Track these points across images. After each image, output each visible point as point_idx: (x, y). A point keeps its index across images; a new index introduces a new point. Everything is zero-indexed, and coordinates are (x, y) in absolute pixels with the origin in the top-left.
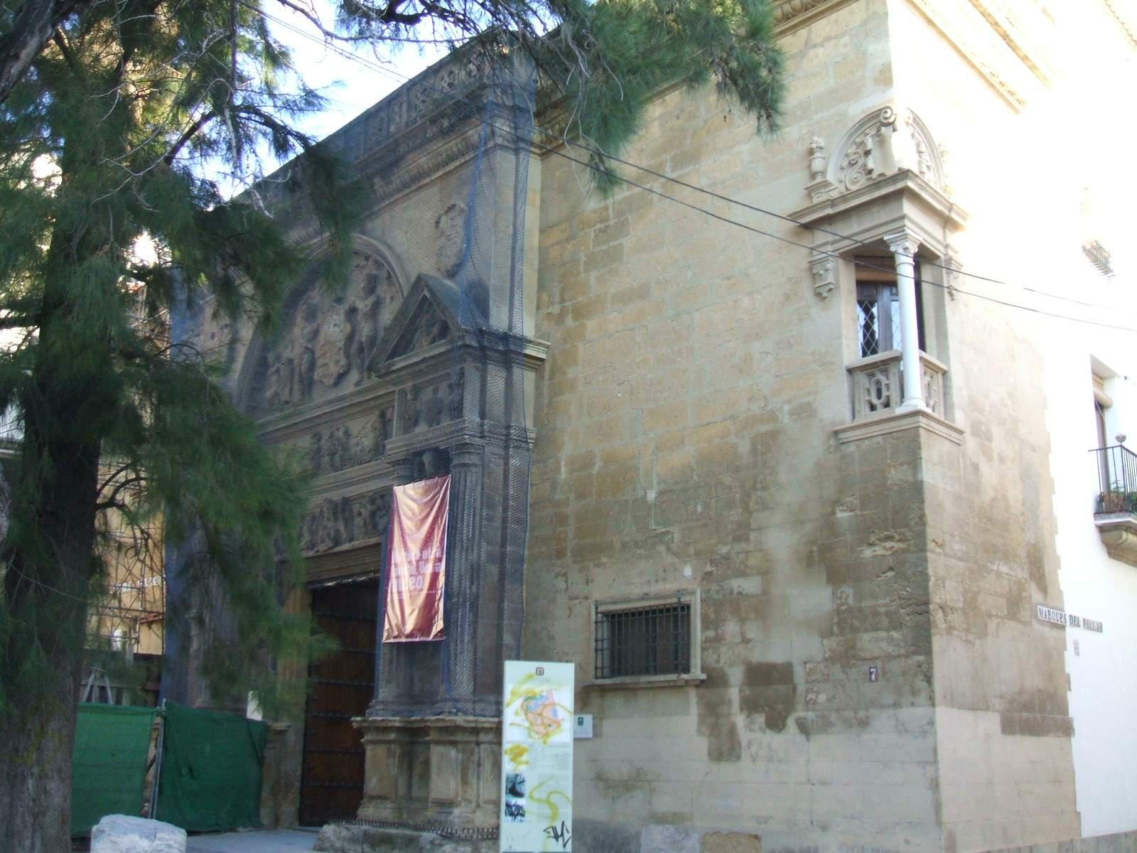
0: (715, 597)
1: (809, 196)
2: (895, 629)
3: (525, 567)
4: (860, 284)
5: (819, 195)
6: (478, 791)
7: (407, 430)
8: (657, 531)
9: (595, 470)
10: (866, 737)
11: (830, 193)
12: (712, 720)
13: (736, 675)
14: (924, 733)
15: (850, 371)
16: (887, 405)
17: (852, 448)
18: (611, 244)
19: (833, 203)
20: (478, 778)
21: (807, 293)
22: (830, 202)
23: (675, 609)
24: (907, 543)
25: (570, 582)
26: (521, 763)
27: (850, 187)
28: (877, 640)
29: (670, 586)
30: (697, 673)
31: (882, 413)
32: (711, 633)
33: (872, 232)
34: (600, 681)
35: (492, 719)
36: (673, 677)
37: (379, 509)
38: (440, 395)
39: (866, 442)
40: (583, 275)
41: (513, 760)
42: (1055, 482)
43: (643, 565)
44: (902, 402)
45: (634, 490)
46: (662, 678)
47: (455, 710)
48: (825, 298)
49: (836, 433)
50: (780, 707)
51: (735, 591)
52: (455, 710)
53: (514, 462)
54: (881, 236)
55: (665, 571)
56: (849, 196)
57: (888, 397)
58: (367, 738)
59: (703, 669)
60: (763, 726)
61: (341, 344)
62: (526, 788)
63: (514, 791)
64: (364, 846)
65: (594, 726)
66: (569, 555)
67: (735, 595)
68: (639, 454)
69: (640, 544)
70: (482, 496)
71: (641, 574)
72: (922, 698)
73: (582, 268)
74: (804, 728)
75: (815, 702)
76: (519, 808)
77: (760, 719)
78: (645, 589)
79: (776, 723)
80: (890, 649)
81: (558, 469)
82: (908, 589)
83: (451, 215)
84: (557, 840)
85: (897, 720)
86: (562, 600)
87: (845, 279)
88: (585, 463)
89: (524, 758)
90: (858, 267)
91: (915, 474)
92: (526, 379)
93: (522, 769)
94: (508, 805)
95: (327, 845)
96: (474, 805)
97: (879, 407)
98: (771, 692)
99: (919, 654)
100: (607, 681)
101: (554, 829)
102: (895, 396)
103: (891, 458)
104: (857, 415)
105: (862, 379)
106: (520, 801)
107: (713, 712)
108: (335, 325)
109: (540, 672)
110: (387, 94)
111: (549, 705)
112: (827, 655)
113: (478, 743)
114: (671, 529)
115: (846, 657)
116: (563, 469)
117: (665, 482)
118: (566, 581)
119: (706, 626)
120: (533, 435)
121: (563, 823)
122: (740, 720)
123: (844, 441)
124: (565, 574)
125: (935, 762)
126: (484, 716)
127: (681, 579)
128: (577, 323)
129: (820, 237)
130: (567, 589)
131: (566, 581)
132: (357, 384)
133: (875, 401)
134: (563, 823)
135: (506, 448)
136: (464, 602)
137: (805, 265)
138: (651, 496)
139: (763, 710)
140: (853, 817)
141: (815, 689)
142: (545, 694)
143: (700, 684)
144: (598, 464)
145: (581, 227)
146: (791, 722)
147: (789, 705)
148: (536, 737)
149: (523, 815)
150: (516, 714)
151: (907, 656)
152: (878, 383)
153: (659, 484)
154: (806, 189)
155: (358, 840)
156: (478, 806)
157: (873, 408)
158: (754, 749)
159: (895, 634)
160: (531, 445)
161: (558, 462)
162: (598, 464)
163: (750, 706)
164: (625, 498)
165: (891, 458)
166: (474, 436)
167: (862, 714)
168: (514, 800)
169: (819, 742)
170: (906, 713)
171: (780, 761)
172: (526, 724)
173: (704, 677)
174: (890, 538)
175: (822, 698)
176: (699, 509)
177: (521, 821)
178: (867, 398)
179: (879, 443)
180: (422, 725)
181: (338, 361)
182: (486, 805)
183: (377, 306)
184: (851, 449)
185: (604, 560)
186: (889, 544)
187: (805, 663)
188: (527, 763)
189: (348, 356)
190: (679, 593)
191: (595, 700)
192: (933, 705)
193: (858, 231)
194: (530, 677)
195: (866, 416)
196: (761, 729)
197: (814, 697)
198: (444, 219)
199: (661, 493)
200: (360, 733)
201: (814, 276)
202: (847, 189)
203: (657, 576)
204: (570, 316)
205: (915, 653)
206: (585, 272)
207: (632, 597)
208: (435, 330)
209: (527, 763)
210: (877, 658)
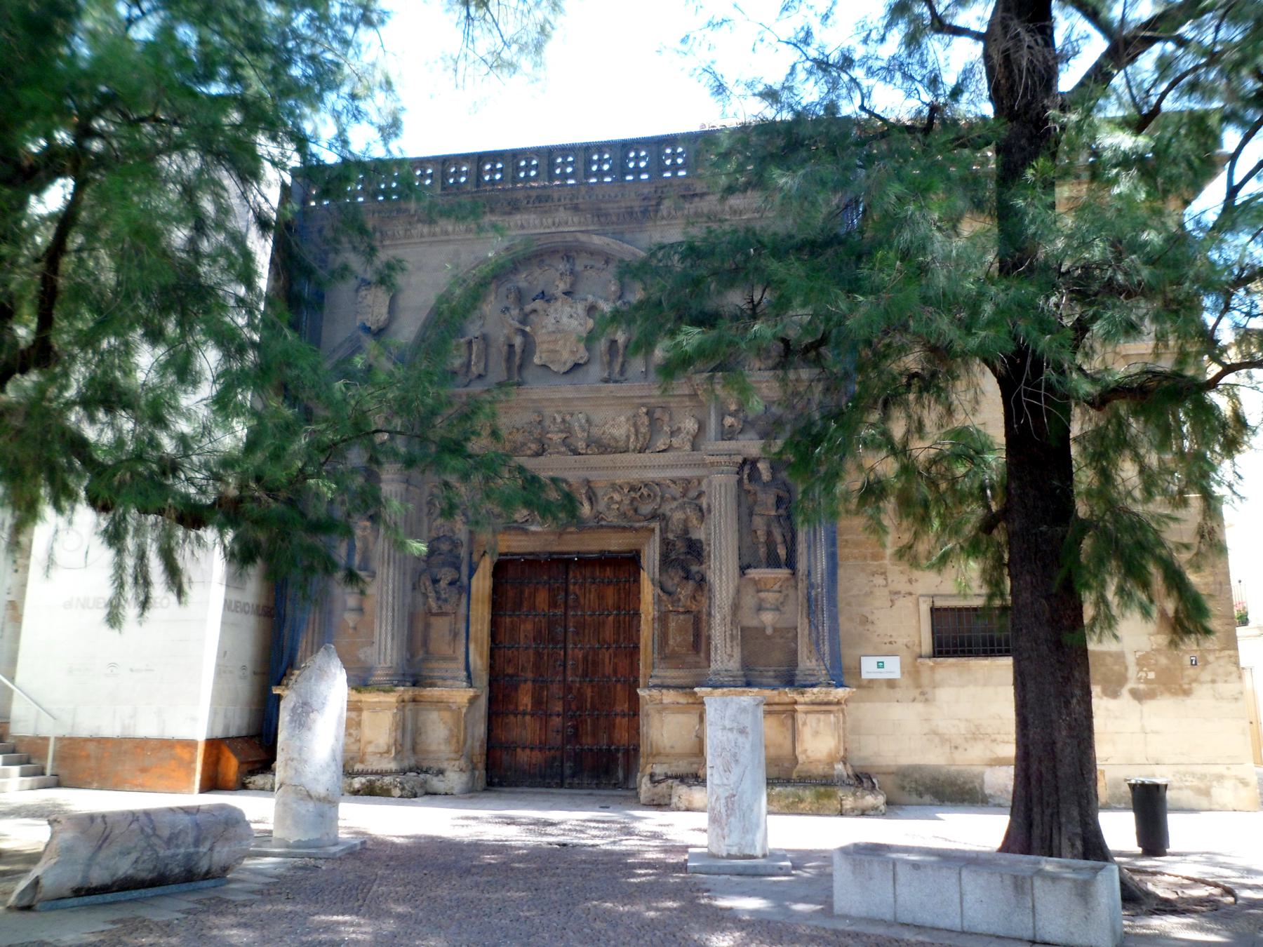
118: (886, 579)
124: (884, 573)
130: (886, 586)
131: (886, 579)
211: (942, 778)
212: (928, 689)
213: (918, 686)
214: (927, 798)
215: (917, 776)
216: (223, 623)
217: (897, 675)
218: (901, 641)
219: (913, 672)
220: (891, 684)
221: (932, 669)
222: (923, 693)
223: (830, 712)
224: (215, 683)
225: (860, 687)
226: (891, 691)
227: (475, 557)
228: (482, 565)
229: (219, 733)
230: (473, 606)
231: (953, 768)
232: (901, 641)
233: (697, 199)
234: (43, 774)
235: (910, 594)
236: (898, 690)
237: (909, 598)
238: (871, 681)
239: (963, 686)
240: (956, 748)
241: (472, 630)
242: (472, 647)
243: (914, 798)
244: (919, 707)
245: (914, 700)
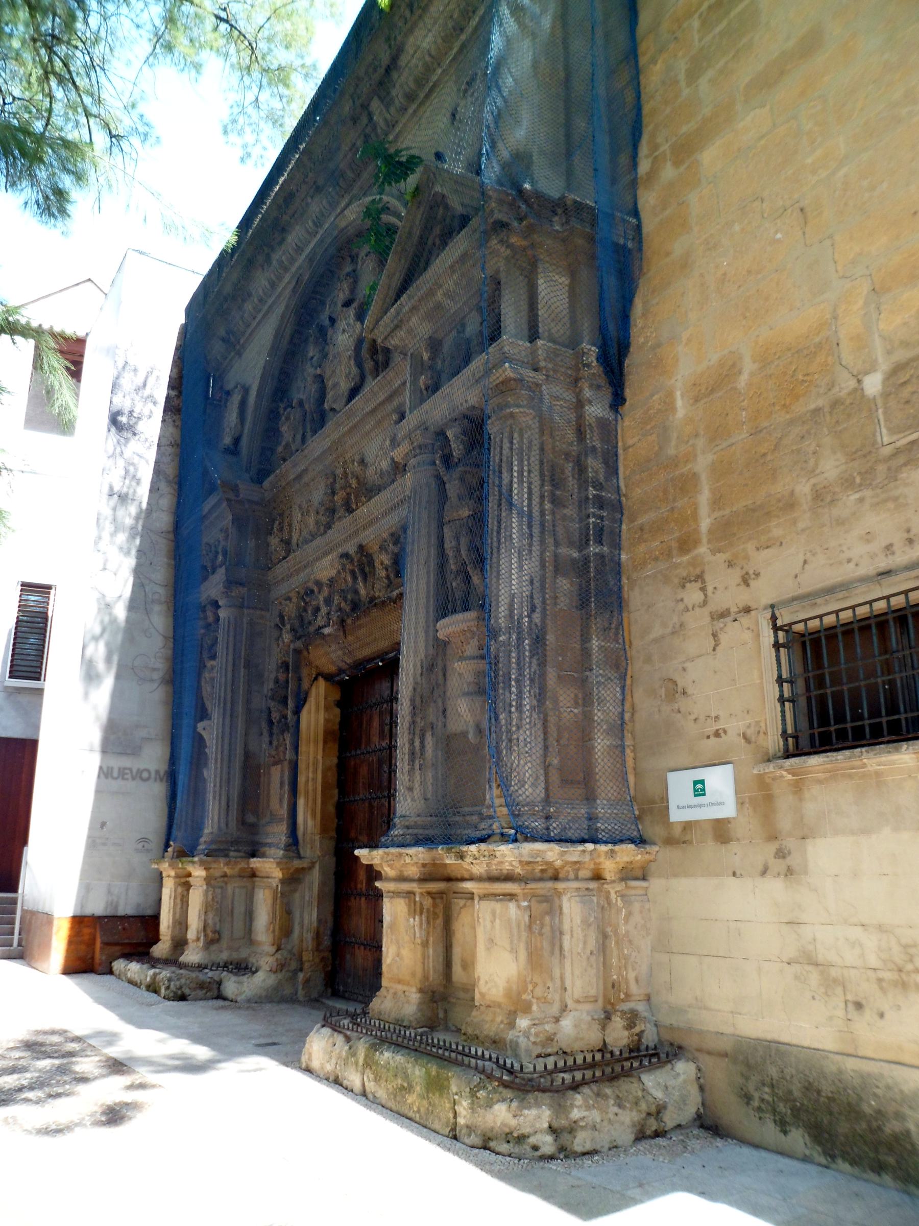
3: (624, 527)
6: (562, 979)
8: (898, 444)
18: (732, 14)
25: (710, 589)
40: (686, 92)
42: (237, 224)
69: (858, 480)
70: (541, 463)
71: (868, 537)
73: (683, 83)
81: (669, 406)
86: (698, 621)
88: (717, 384)
110: (358, 12)
116: (679, 403)
118: (703, 589)
124: (700, 577)
128: (682, 168)
130: (705, 603)
131: (703, 589)
136: (520, 640)
138: (873, 384)
144: (748, 366)
153: (889, 353)
161: (670, 394)
162: (748, 366)
182: (580, 1007)
185: (777, 532)
187: (763, 217)
203: (908, 531)
204: (669, 164)
206: (689, 85)
211: (827, 1089)
212: (790, 843)
213: (773, 836)
214: (798, 1138)
215: (773, 1071)
216: (98, 791)
217: (728, 810)
218: (734, 726)
219: (758, 798)
220: (721, 831)
221: (798, 788)
222: (781, 854)
223: (511, 896)
224: (86, 856)
225: (670, 841)
226: (723, 848)
227: (305, 685)
228: (313, 691)
229: (97, 907)
230: (303, 748)
231: (850, 1064)
232: (734, 726)
233: (395, 75)
234: (11, 946)
235: (747, 610)
236: (734, 846)
237: (745, 620)
238: (688, 826)
239: (865, 831)
240: (859, 1006)
241: (302, 779)
242: (301, 802)
243: (769, 1131)
244: (775, 886)
245: (764, 872)
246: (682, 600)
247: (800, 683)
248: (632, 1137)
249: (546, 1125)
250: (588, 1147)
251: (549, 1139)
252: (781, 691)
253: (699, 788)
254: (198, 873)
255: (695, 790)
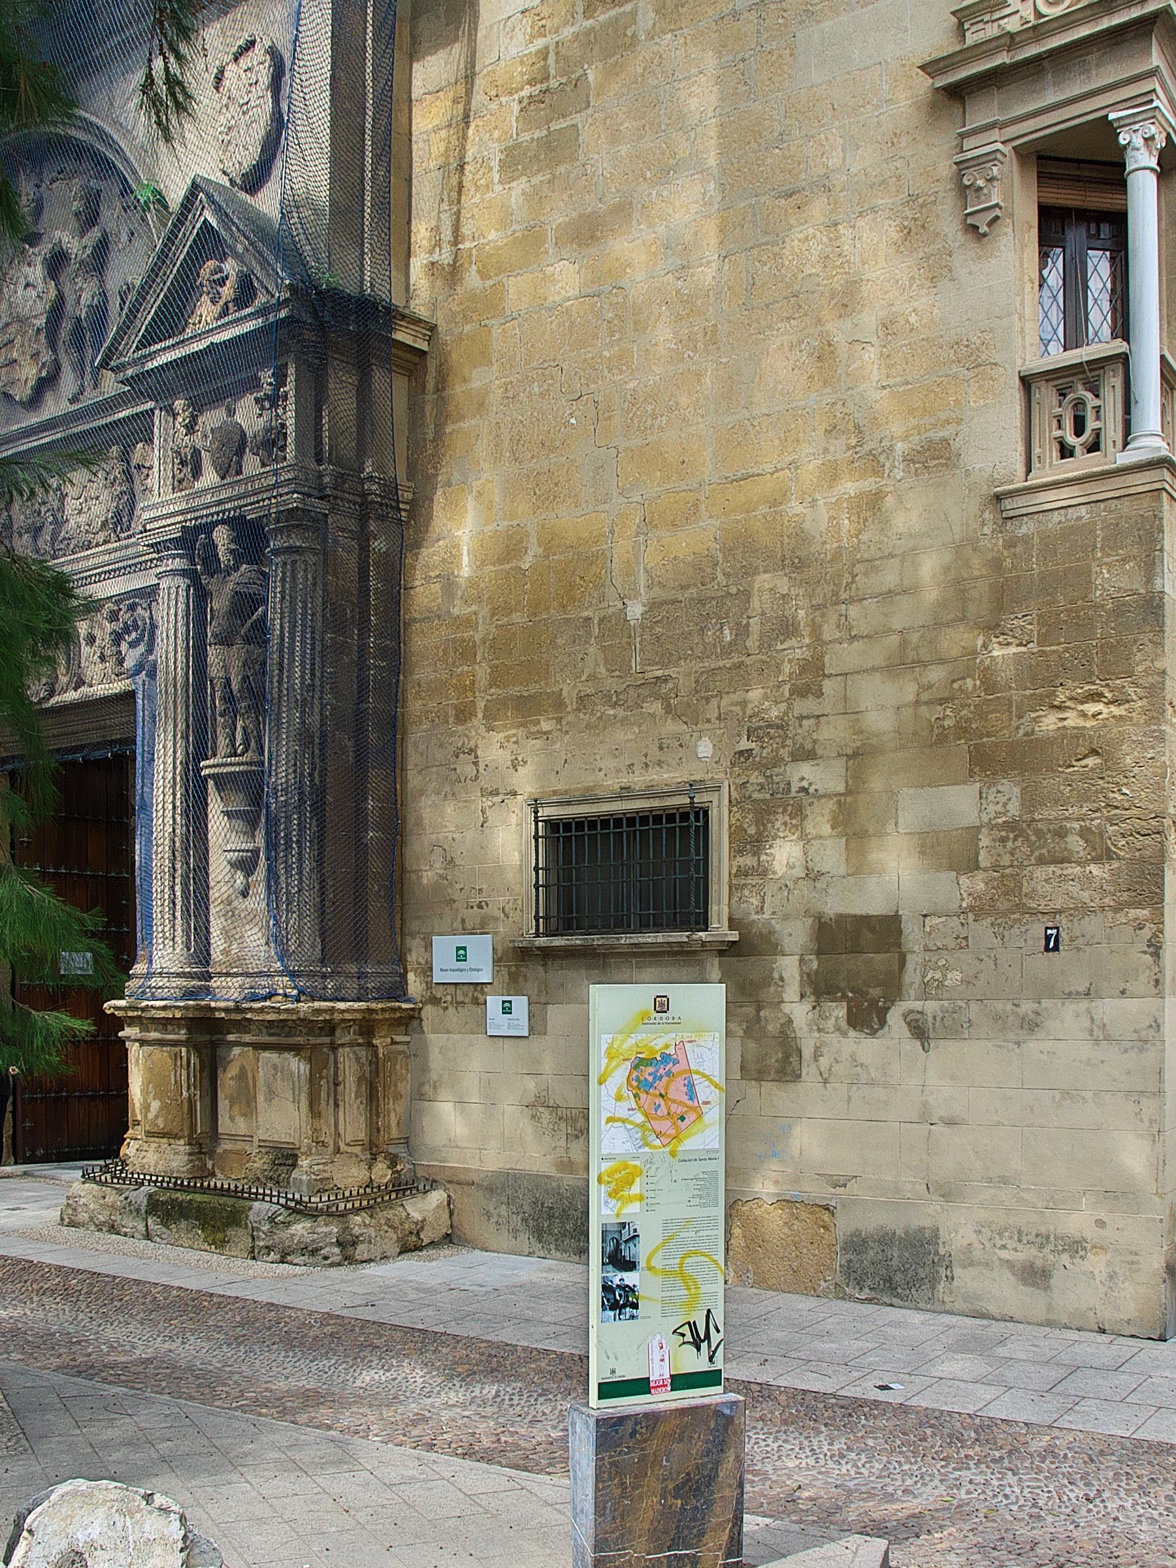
0: (756, 795)
1: (961, 31)
2: (1096, 860)
4: (1046, 213)
5: (981, 26)
6: (336, 1125)
7: (179, 484)
9: (526, 563)
10: (1033, 1046)
11: (1002, 22)
12: (750, 1010)
13: (795, 936)
14: (1143, 1043)
15: (1027, 382)
16: (1094, 447)
17: (1026, 528)
19: (1011, 40)
20: (337, 1105)
21: (949, 226)
22: (1006, 40)
23: (685, 816)
24: (1127, 706)
26: (630, 1199)
27: (1044, 9)
28: (1063, 878)
29: (670, 776)
30: (719, 929)
31: (1083, 464)
32: (748, 861)
33: (1025, 124)
34: (542, 941)
35: (356, 1005)
36: (681, 936)
37: (127, 630)
38: (238, 418)
39: (1056, 517)
41: (613, 1194)
43: (620, 735)
44: (1126, 444)
45: (602, 598)
46: (649, 938)
47: (295, 992)
48: (985, 235)
49: (998, 498)
50: (875, 992)
51: (795, 787)
52: (295, 992)
53: (378, 545)
54: (1103, 113)
55: (661, 748)
56: (1047, 28)
57: (1097, 433)
58: (128, 1032)
59: (733, 924)
60: (843, 1024)
61: (41, 322)
62: (641, 1251)
63: (618, 1260)
64: (150, 1221)
65: (531, 1016)
66: (480, 715)
67: (793, 794)
68: (612, 532)
71: (616, 752)
72: (1141, 984)
74: (919, 1031)
75: (941, 985)
76: (629, 1290)
77: (839, 1011)
78: (625, 781)
79: (866, 1017)
80: (1085, 896)
82: (1125, 790)
83: (244, 62)
84: (699, 1349)
85: (1092, 1019)
87: (1017, 199)
89: (635, 1189)
90: (1043, 178)
91: (1149, 580)
92: (393, 392)
93: (631, 1211)
94: (607, 1288)
95: (83, 1217)
96: (331, 1148)
97: (1078, 451)
98: (861, 965)
99: (1139, 905)
100: (558, 942)
101: (692, 1326)
102: (1113, 433)
103: (1102, 549)
104: (1035, 464)
105: (1046, 395)
106: (630, 1278)
107: (749, 1001)
108: (27, 285)
109: (662, 1005)
111: (680, 1073)
112: (964, 905)
113: (334, 1048)
114: (671, 671)
115: (1005, 903)
116: (465, 560)
117: (662, 586)
119: (738, 850)
120: (408, 496)
121: (709, 1311)
122: (799, 1011)
123: (1011, 514)
124: (472, 751)
125: (1160, 1093)
126: (343, 1000)
127: (688, 762)
129: (982, 112)
132: (74, 400)
133: (1071, 439)
134: (709, 1311)
135: (363, 520)
137: (945, 169)
138: (635, 611)
139: (844, 997)
140: (1004, 1181)
141: (942, 962)
142: (671, 1051)
143: (728, 950)
145: (494, 93)
146: (895, 1017)
147: (893, 988)
148: (657, 1142)
149: (635, 1306)
150: (619, 1098)
151: (1116, 910)
152: (1079, 404)
153: (649, 587)
154: (953, 13)
155: (138, 1210)
156: (338, 1151)
157: (1066, 452)
158: (824, 1062)
159: (1095, 869)
160: (403, 514)
163: (820, 988)
164: (585, 614)
165: (1102, 549)
166: (309, 496)
167: (1027, 1007)
168: (617, 1277)
169: (944, 1052)
170: (1108, 1008)
171: (872, 1083)
172: (639, 1118)
173: (734, 936)
174: (1095, 697)
175: (954, 977)
176: (728, 635)
177: (632, 1317)
178: (1059, 433)
179: (1079, 518)
180: (239, 1017)
181: (38, 354)
183: (102, 249)
184: (1024, 530)
186: (1091, 708)
188: (641, 1198)
189: (52, 344)
190: (693, 787)
191: (535, 971)
192: (1161, 996)
193: (1051, 107)
194: (644, 1018)
195: (1051, 468)
196: (838, 1029)
197: (938, 975)
198: (231, 70)
199: (653, 606)
200: (118, 1023)
201: (963, 191)
202: (1038, 15)
205: (1131, 904)
207: (601, 793)
208: (227, 292)
209: (641, 1198)
210: (1060, 912)
246: (455, 769)
247: (553, 873)
248: (155, 1497)
249: (334, 1240)
250: (366, 1257)
251: (337, 1250)
252: (537, 878)
253: (461, 954)
254: (231, 1037)
255: (504, 1008)
